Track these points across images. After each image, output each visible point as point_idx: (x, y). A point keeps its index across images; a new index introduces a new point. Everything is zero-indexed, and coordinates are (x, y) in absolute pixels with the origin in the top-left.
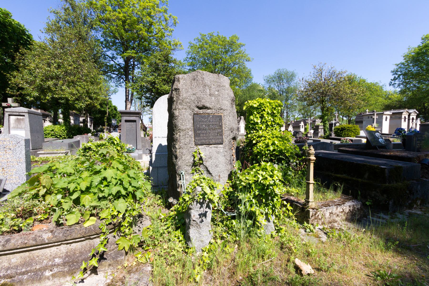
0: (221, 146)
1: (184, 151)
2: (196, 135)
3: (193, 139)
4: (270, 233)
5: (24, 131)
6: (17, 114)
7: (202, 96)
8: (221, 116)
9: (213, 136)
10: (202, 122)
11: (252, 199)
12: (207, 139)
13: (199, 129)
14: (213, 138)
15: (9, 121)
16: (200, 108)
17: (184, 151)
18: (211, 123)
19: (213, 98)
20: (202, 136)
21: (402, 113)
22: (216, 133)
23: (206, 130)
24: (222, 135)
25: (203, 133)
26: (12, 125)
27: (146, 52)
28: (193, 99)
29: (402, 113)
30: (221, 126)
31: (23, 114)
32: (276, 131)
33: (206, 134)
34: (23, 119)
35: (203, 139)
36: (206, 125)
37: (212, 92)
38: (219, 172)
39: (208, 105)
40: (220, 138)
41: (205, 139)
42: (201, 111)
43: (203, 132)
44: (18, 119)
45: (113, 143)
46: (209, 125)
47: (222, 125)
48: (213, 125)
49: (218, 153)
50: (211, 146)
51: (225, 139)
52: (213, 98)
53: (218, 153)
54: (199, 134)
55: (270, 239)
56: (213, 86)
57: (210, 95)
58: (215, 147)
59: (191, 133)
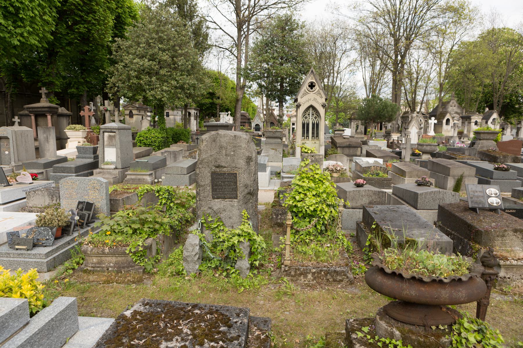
0: (236, 200)
1: (203, 203)
2: (214, 190)
3: (211, 194)
5: (115, 149)
6: (110, 130)
7: (218, 157)
8: (236, 174)
13: (216, 185)
15: (103, 138)
16: (217, 167)
17: (203, 203)
19: (229, 158)
23: (221, 186)
24: (236, 191)
26: (106, 143)
28: (210, 159)
30: (236, 183)
31: (115, 130)
32: (76, 261)
34: (114, 136)
36: (222, 182)
37: (228, 152)
38: (232, 223)
39: (223, 164)
42: (218, 170)
44: (110, 136)
45: (115, 232)
46: (224, 182)
47: (237, 181)
48: (228, 181)
49: (232, 206)
50: (226, 200)
51: (239, 195)
52: (229, 158)
53: (232, 206)
54: (216, 189)
56: (228, 147)
57: (226, 155)
58: (229, 201)
59: (209, 188)
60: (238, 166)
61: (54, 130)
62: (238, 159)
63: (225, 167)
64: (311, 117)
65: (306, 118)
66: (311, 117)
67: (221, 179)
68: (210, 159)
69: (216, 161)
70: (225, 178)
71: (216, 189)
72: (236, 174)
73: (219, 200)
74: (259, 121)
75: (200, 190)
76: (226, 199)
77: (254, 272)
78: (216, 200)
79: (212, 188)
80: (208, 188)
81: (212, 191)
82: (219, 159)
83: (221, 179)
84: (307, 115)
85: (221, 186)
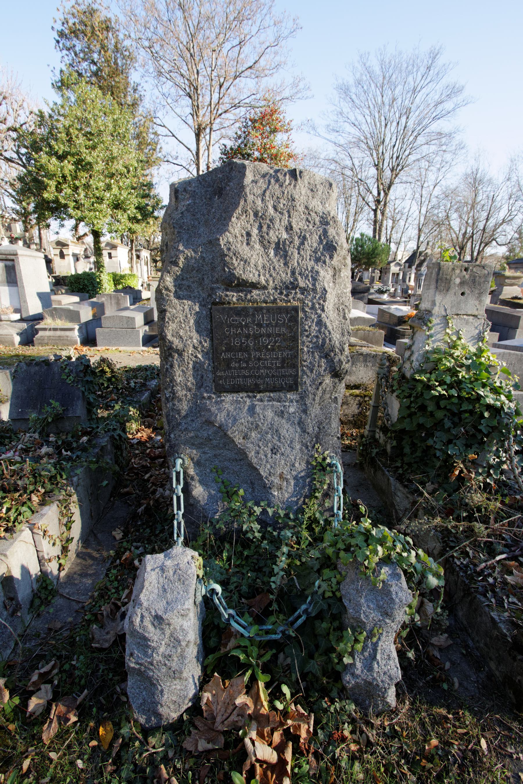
4: (283, 59)
9: (268, 368)
10: (237, 327)
11: (163, 643)
12: (250, 377)
14: (267, 376)
18: (263, 330)
20: (235, 368)
21: (242, 775)
22: (277, 359)
24: (295, 366)
25: (240, 360)
27: (470, 631)
29: (242, 775)
33: (247, 362)
35: (239, 376)
40: (291, 376)
41: (245, 377)
43: (240, 355)
48: (269, 336)
55: (333, 182)
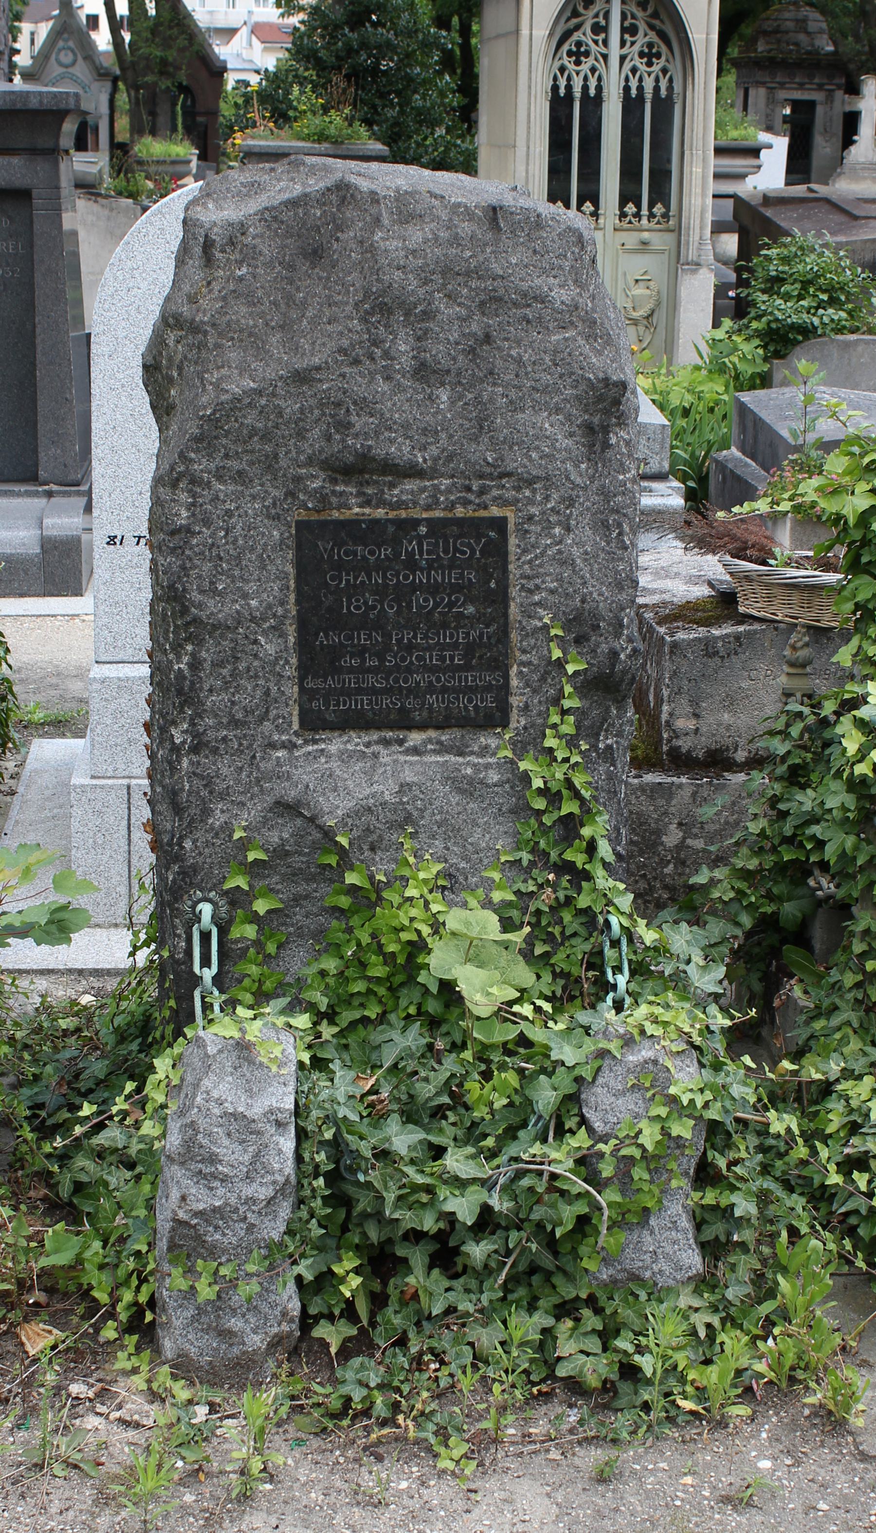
1: (225, 767)
8: (500, 524)
17: (225, 767)
23: (379, 625)
24: (501, 666)
28: (291, 407)
30: (502, 598)
46: (403, 594)
48: (434, 589)
50: (415, 738)
54: (335, 653)
56: (440, 303)
58: (443, 749)
60: (515, 461)
61: (201, 25)
62: (515, 407)
63: (413, 472)
64: (615, 51)
65: (579, 54)
66: (615, 51)
67: (381, 567)
68: (291, 407)
69: (344, 426)
70: (412, 565)
71: (335, 653)
72: (500, 524)
73: (356, 741)
74: (81, 70)
75: (195, 665)
76: (410, 727)
77: (462, 1056)
78: (335, 744)
79: (304, 645)
80: (269, 647)
81: (304, 670)
82: (364, 405)
83: (381, 567)
84: (585, 35)
85: (379, 625)
